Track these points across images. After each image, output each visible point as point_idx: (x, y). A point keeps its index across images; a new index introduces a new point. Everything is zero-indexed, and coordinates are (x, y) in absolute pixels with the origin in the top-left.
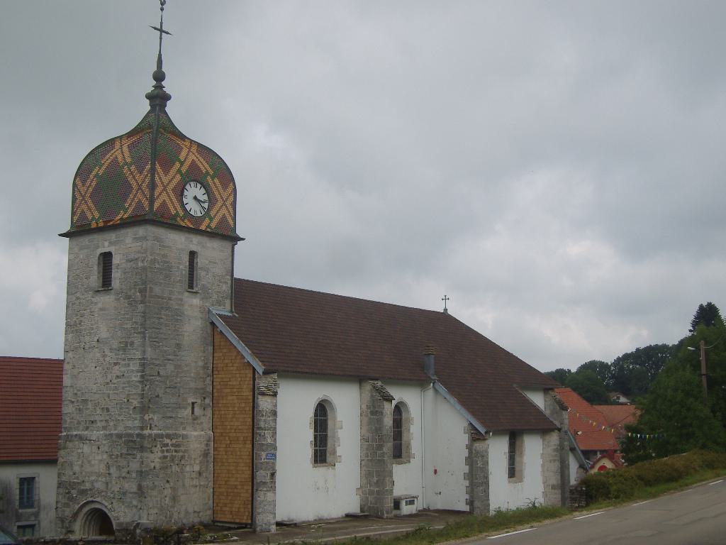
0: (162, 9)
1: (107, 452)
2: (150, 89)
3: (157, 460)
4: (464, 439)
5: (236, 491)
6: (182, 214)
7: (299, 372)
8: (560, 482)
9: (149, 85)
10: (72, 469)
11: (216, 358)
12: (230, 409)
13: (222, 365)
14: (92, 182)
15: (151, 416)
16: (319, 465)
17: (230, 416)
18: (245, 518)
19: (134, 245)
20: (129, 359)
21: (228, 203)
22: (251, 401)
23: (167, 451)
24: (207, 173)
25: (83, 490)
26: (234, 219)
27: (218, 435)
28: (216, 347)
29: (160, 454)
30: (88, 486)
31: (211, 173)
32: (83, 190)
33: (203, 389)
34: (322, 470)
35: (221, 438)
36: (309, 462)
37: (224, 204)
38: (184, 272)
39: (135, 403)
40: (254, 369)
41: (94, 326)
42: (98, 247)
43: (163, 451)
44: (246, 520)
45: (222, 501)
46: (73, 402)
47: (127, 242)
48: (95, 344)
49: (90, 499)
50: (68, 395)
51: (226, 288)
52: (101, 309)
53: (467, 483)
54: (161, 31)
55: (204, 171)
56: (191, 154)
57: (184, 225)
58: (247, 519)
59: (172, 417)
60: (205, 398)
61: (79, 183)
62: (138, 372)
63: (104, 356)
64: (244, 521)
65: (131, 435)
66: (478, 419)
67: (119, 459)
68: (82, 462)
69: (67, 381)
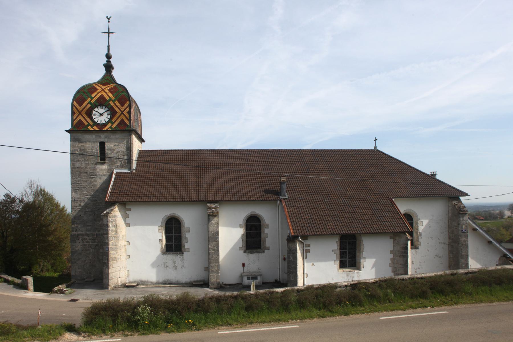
0: (109, 22)
2: (105, 62)
3: (80, 246)
6: (91, 123)
9: (105, 61)
15: (76, 225)
21: (125, 113)
29: (81, 244)
43: (84, 242)
54: (109, 33)
57: (92, 129)
59: (90, 226)
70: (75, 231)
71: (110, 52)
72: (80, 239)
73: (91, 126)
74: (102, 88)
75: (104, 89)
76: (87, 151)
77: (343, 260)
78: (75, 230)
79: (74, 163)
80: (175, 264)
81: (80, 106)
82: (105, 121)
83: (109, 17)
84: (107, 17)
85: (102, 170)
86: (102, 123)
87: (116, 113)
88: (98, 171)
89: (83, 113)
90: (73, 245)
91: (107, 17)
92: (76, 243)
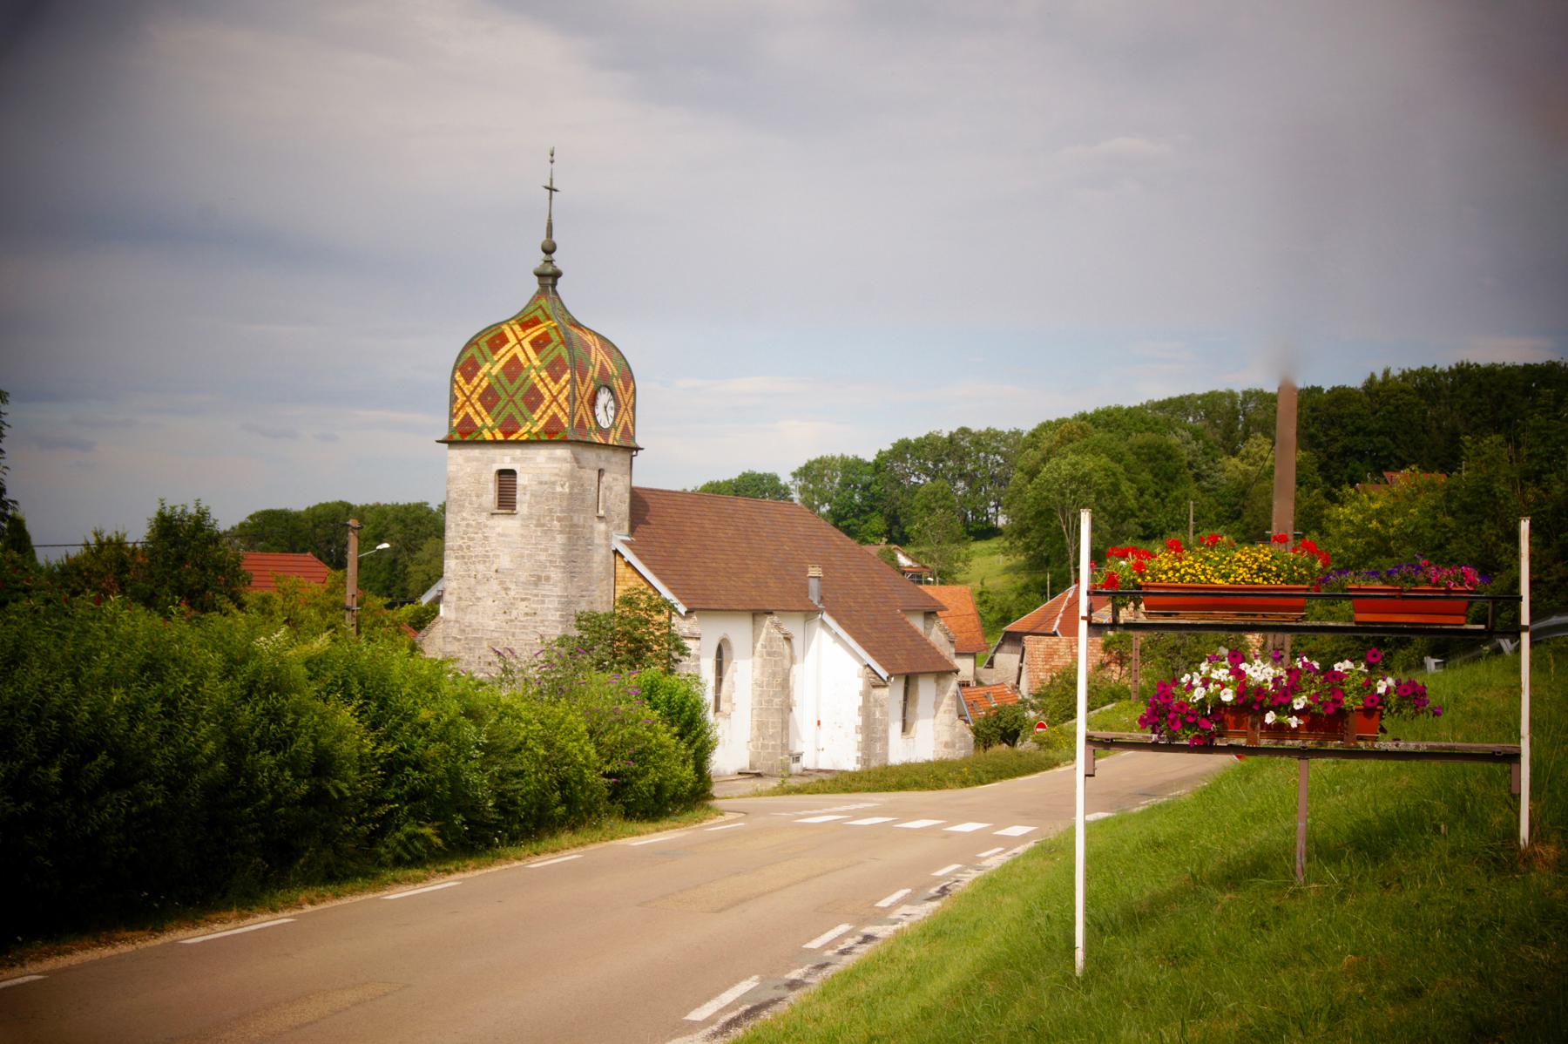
0: (552, 162)
16: (755, 719)
19: (548, 466)
20: (544, 596)
26: (634, 425)
28: (618, 579)
41: (491, 554)
42: (494, 461)
46: (459, 640)
47: (538, 460)
48: (493, 574)
52: (499, 535)
53: (860, 737)
62: (557, 610)
63: (507, 589)
66: (878, 661)
71: (555, 238)
74: (551, 403)
75: (552, 394)
77: (1473, 623)
84: (556, 190)
89: (517, 398)
91: (556, 190)
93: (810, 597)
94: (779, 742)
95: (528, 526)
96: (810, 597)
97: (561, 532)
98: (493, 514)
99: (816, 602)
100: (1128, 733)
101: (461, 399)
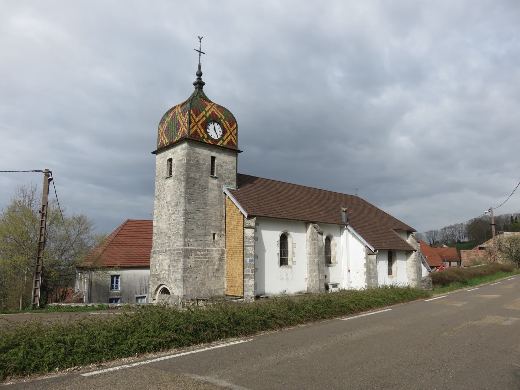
0: (200, 42)
1: (169, 259)
4: (364, 254)
5: (236, 279)
6: (206, 137)
7: (269, 217)
8: (416, 278)
9: (195, 79)
10: (156, 268)
11: (227, 211)
12: (233, 236)
13: (230, 214)
14: (165, 126)
15: (189, 239)
17: (233, 240)
18: (240, 293)
21: (233, 133)
22: (243, 232)
23: (198, 258)
24: (221, 118)
25: (159, 278)
27: (228, 250)
28: (227, 205)
29: (194, 259)
30: (161, 276)
31: (224, 118)
32: (162, 130)
33: (219, 226)
34: (284, 268)
35: (230, 252)
36: (277, 264)
37: (231, 134)
38: (208, 167)
39: (181, 233)
40: (244, 216)
43: (196, 258)
44: (240, 295)
45: (230, 284)
49: (162, 283)
50: (155, 231)
51: (234, 176)
52: (168, 187)
53: (366, 277)
54: (200, 52)
55: (219, 117)
56: (212, 108)
57: (207, 142)
58: (241, 294)
59: (201, 240)
60: (221, 231)
61: (160, 127)
63: (169, 210)
64: (240, 295)
65: (178, 249)
66: (370, 244)
67: (174, 262)
68: (160, 264)
69: (155, 224)
70: (187, 246)
71: (202, 70)
72: (193, 254)
73: (206, 139)
76: (201, 163)
78: (187, 244)
79: (189, 173)
80: (288, 277)
81: (197, 117)
82: (211, 136)
83: (200, 37)
84: (199, 37)
85: (213, 184)
86: (215, 138)
87: (227, 132)
88: (210, 184)
90: (186, 261)
91: (199, 37)
92: (189, 258)
93: (343, 220)
94: (318, 279)
95: (175, 181)
96: (343, 220)
97: (184, 181)
98: (166, 178)
99: (345, 222)
100: (171, 116)
101: (161, 134)
